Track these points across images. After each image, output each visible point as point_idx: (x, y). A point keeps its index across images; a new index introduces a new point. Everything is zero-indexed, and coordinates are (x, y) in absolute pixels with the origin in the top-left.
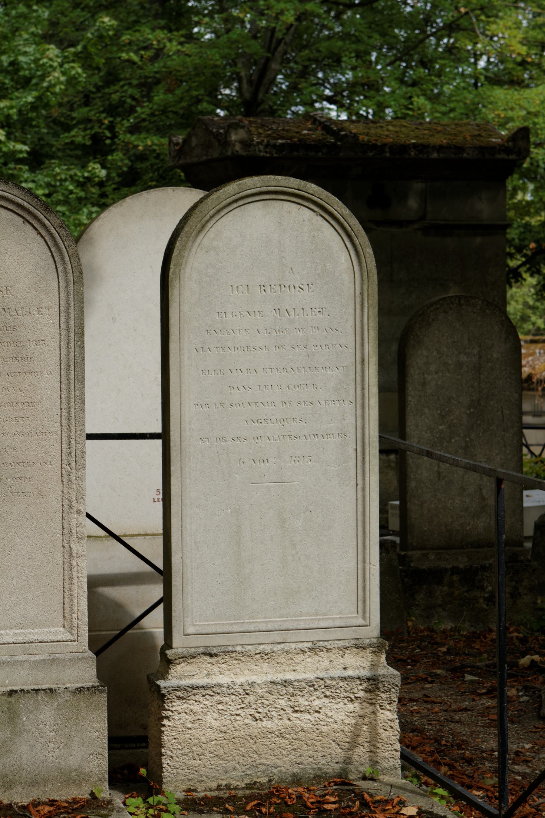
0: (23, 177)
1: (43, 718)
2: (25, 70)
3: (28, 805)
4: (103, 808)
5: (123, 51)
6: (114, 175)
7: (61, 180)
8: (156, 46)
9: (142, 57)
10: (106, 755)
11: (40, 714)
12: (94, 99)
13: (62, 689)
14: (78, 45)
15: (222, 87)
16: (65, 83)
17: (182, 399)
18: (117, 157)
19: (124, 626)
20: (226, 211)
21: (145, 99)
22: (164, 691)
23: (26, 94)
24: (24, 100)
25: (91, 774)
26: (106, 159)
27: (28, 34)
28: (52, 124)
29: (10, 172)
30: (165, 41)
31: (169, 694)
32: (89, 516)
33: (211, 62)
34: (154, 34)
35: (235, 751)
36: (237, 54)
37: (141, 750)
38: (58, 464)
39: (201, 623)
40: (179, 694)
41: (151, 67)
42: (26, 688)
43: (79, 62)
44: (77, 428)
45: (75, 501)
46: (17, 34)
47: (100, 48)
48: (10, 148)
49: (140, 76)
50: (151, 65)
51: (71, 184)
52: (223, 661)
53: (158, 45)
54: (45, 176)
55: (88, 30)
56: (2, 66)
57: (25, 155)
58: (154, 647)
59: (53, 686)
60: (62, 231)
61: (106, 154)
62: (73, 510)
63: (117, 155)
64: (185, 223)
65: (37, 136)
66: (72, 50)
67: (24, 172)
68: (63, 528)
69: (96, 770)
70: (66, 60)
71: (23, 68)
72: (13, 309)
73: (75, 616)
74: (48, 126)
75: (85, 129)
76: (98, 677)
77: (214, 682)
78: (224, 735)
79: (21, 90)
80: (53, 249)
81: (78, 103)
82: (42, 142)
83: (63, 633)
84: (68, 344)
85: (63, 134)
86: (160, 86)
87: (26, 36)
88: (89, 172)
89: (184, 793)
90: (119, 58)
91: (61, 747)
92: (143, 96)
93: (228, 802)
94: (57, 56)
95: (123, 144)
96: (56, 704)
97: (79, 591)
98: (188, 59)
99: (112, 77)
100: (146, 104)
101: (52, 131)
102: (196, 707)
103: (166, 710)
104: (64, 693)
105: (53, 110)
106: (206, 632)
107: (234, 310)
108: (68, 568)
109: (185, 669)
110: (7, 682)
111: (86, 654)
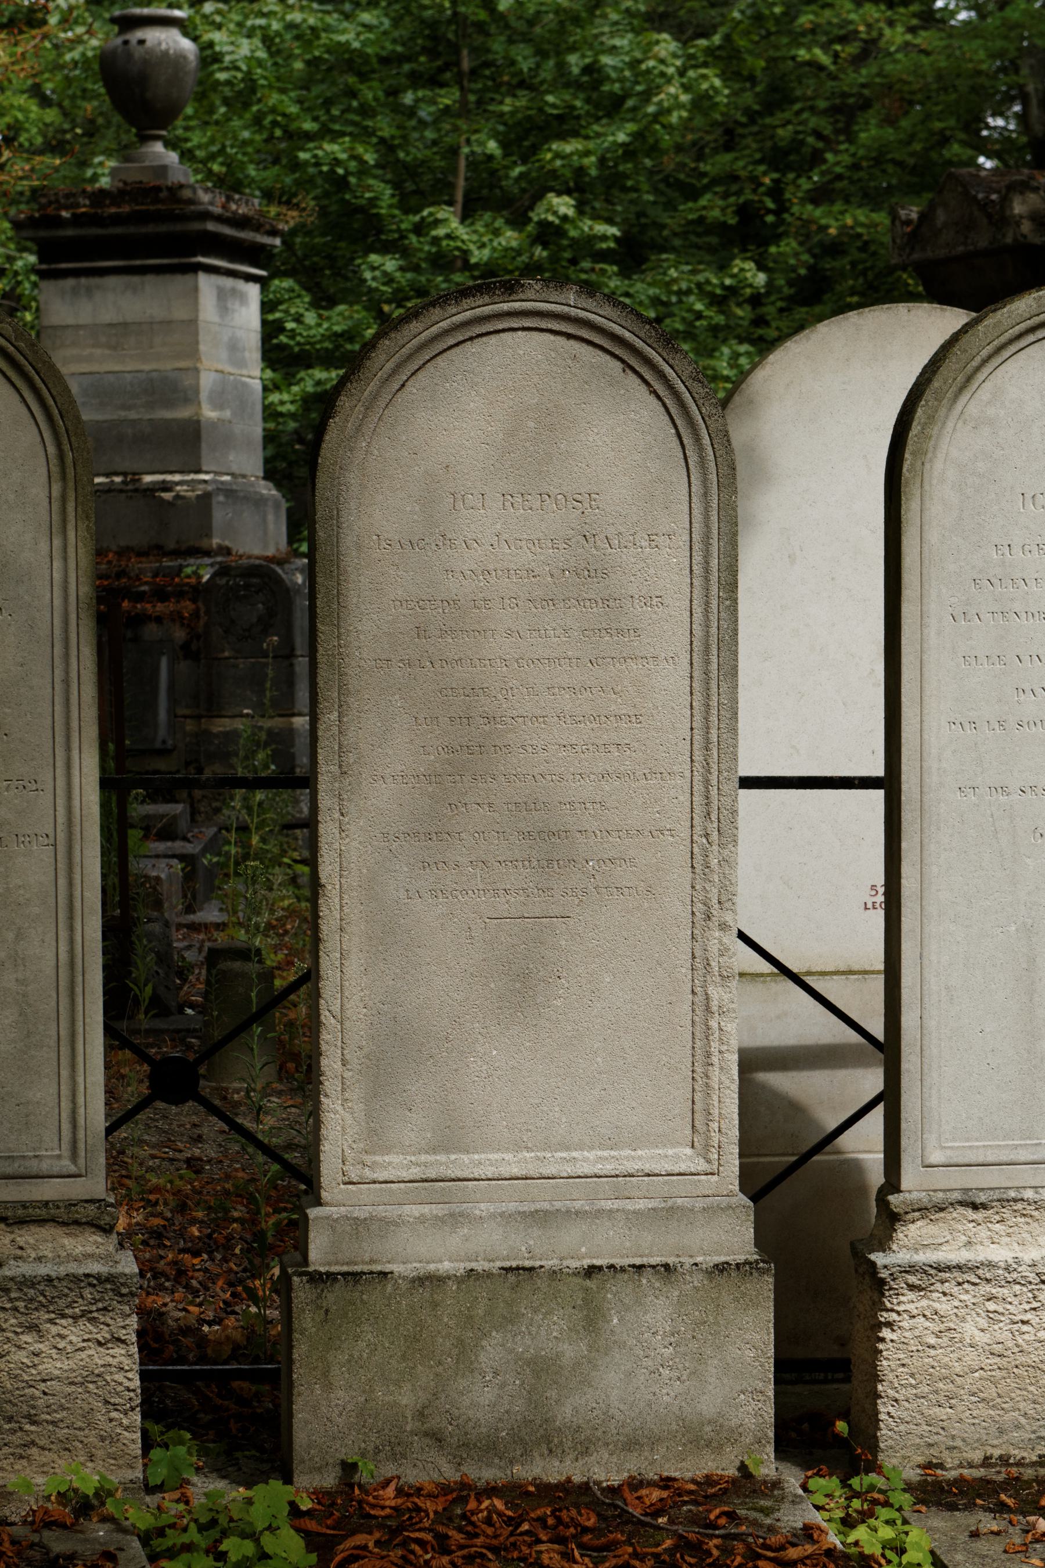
0: (607, 286)
1: (650, 1321)
2: (614, 81)
3: (620, 1486)
4: (765, 1496)
5: (800, 45)
6: (782, 282)
7: (680, 293)
8: (863, 36)
9: (836, 55)
10: (771, 1394)
11: (645, 1313)
12: (743, 136)
13: (687, 1266)
14: (715, 32)
15: (989, 112)
16: (689, 107)
17: (925, 711)
18: (787, 247)
19: (805, 1148)
20: (1013, 348)
21: (842, 138)
22: (884, 1274)
23: (614, 128)
24: (611, 138)
25: (740, 1430)
26: (766, 251)
27: (619, 12)
28: (662, 186)
29: (584, 276)
30: (882, 25)
31: (894, 1280)
32: (742, 936)
33: (970, 66)
34: (861, 11)
35: (1018, 1392)
36: (1020, 49)
37: (835, 1386)
38: (686, 834)
39: (956, 1144)
40: (912, 1279)
41: (853, 75)
42: (618, 1262)
43: (714, 66)
44: (723, 767)
45: (717, 906)
46: (598, 13)
47: (756, 38)
48: (583, 231)
49: (833, 93)
50: (855, 71)
51: (700, 300)
52: (997, 1218)
53: (868, 33)
54: (649, 284)
55: (732, 4)
56: (570, 73)
57: (612, 245)
58: (862, 1189)
59: (671, 1260)
60: (697, 387)
61: (766, 243)
62: (714, 924)
63: (787, 245)
64: (934, 373)
65: (633, 209)
66: (703, 42)
67: (610, 278)
68: (694, 957)
69: (750, 1422)
70: (691, 61)
71: (608, 78)
72: (602, 536)
73: (715, 1126)
74: (656, 191)
75: (725, 196)
76: (756, 1245)
77: (981, 1258)
78: (997, 1360)
79: (604, 121)
80: (678, 422)
81: (712, 145)
82: (643, 220)
83: (690, 1158)
84: (707, 604)
85: (685, 203)
86: (871, 111)
87: (614, 16)
88: (733, 276)
89: (919, 1471)
90: (793, 58)
91: (684, 1377)
92: (837, 132)
93: (1005, 1491)
94: (675, 56)
95: (799, 223)
96: (677, 1293)
97: (723, 1078)
98: (925, 60)
99: (778, 96)
100: (842, 147)
101: (663, 199)
102: (944, 1306)
103: (887, 1310)
104: (691, 1273)
105: (665, 159)
106: (966, 1161)
107: (1028, 541)
108: (702, 1035)
109: (924, 1231)
110: (583, 1250)
111: (734, 1200)
